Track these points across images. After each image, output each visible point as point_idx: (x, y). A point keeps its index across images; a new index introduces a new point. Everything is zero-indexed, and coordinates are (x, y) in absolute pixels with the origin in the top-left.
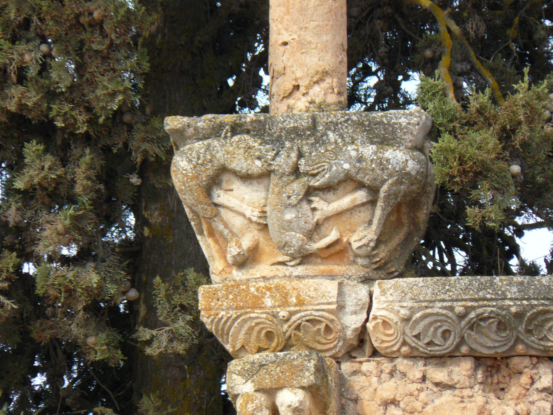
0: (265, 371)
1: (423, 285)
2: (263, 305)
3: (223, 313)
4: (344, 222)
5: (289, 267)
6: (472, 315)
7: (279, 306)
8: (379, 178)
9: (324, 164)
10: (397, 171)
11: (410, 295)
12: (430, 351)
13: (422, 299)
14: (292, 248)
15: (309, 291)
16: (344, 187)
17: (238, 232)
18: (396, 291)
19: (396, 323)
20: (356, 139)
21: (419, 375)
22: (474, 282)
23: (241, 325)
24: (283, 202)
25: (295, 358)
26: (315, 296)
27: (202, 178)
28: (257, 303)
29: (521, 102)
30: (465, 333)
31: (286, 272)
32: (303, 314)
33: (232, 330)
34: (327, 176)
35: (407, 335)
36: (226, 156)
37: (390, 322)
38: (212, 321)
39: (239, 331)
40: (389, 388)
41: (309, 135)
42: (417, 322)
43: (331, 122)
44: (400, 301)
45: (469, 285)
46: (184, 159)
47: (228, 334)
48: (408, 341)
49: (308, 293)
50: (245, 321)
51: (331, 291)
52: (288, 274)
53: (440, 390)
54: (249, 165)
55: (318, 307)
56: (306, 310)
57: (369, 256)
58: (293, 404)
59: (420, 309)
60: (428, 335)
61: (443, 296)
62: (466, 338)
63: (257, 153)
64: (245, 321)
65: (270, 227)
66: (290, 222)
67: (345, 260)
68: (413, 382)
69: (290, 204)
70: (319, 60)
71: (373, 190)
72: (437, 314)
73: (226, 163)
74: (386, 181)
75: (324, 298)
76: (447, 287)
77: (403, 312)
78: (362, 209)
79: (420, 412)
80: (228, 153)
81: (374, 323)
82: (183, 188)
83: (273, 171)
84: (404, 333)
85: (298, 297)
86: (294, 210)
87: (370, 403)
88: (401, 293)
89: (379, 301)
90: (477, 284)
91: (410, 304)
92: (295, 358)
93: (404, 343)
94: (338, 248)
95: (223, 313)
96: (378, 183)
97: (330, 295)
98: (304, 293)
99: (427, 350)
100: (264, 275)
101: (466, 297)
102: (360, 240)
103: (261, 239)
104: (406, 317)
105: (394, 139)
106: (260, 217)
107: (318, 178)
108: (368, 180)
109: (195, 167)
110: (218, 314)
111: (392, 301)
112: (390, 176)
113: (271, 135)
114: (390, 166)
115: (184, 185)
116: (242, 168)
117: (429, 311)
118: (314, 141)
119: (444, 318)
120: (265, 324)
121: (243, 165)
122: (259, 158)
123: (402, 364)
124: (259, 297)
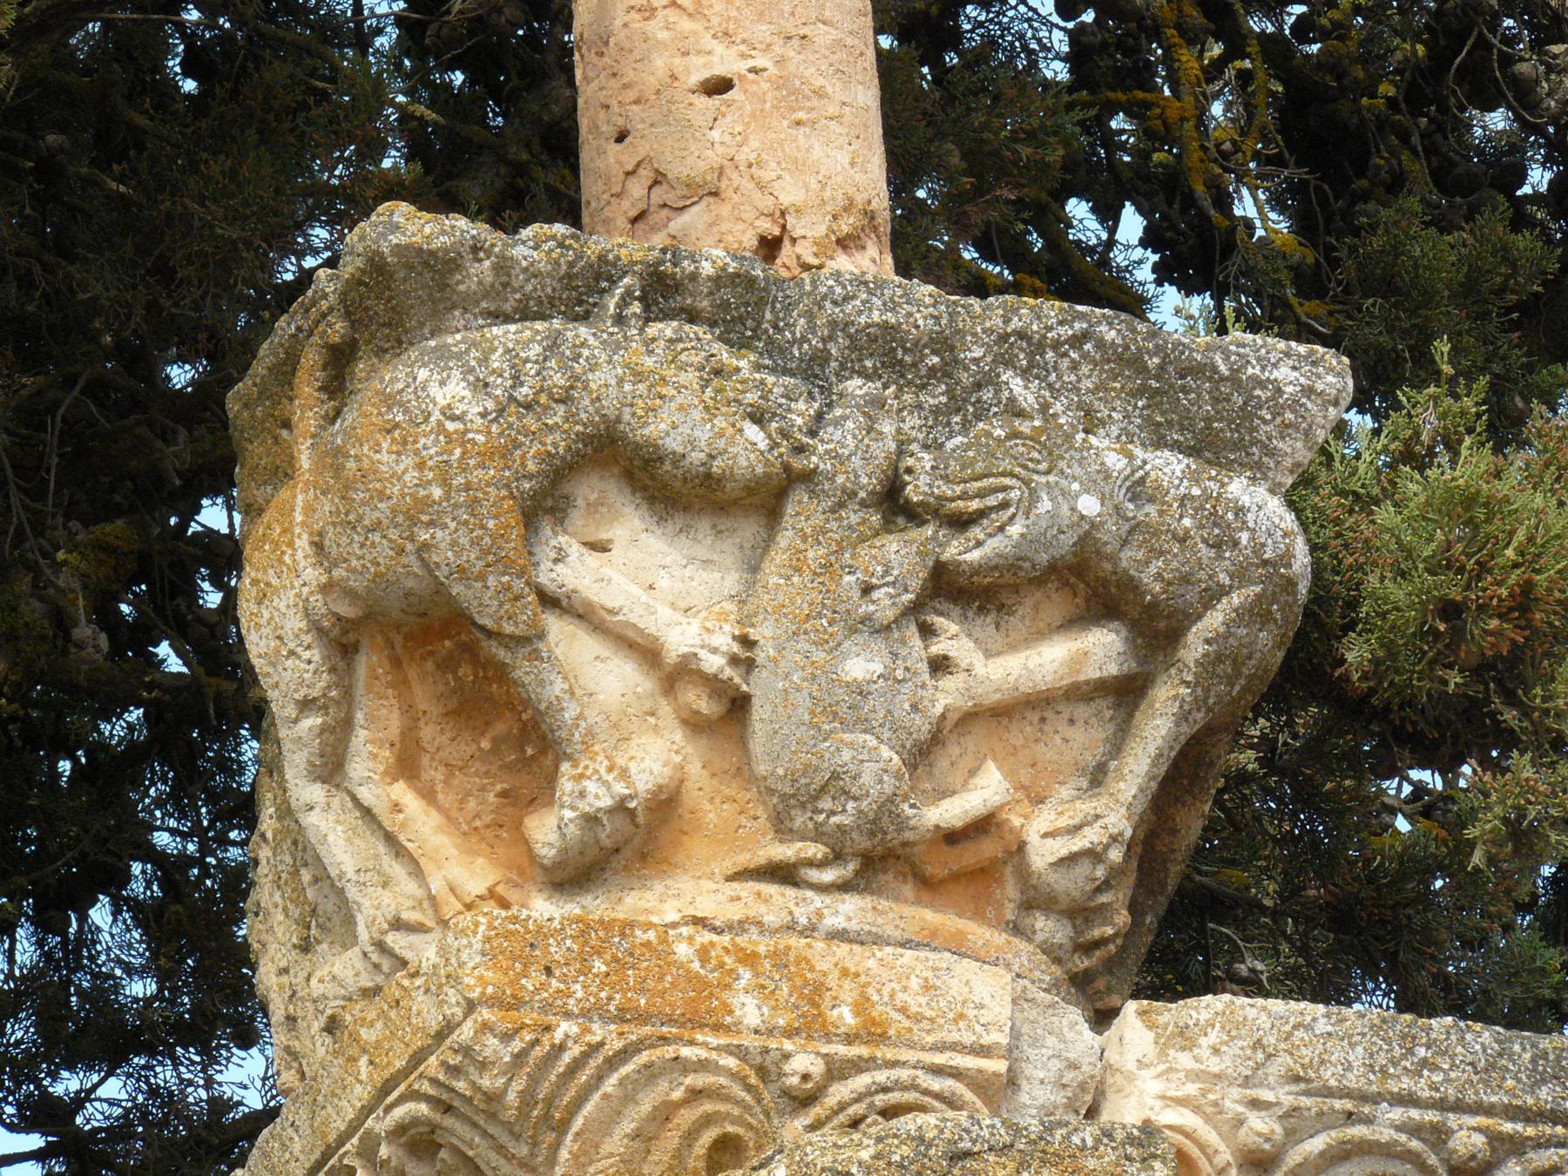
1: (1329, 1028)
2: (729, 1019)
3: (565, 1028)
4: (1015, 751)
5: (809, 894)
7: (790, 1033)
8: (1202, 575)
9: (1008, 481)
10: (1265, 563)
13: (1333, 1083)
14: (851, 805)
15: (905, 989)
16: (1036, 608)
17: (605, 725)
18: (1232, 1038)
20: (1103, 423)
22: (1517, 1048)
23: (628, 1094)
24: (841, 608)
25: (1090, 1142)
26: (929, 1013)
27: (523, 457)
28: (703, 1015)
31: (797, 912)
32: (881, 1076)
33: (589, 1107)
34: (1015, 530)
36: (627, 387)
37: (1203, 1163)
38: (519, 1057)
39: (613, 1115)
41: (932, 370)
43: (1021, 335)
44: (1247, 1082)
45: (1501, 1055)
46: (457, 374)
49: (901, 997)
50: (650, 1073)
51: (987, 1001)
52: (803, 921)
54: (721, 435)
55: (940, 1059)
56: (894, 1064)
57: (1080, 913)
59: (1324, 1121)
61: (1406, 1083)
63: (751, 397)
64: (650, 1073)
65: (760, 713)
66: (860, 691)
67: (990, 913)
69: (866, 619)
70: (852, 164)
71: (1156, 631)
73: (627, 417)
74: (1224, 591)
75: (962, 1024)
76: (1421, 1052)
77: (1259, 1123)
78: (1082, 711)
80: (639, 376)
82: (437, 492)
83: (808, 477)
85: (862, 1006)
86: (879, 644)
88: (1254, 1048)
89: (1170, 1070)
90: (1527, 1056)
91: (1286, 1096)
92: (1090, 1142)
94: (987, 848)
95: (565, 1028)
96: (1192, 595)
97: (986, 1016)
98: (886, 991)
100: (700, 915)
101: (1494, 1099)
103: (695, 769)
104: (1267, 1146)
105: (1237, 446)
106: (734, 660)
107: (976, 532)
108: (1159, 577)
109: (501, 411)
110: (548, 1028)
112: (1240, 576)
113: (782, 351)
114: (1244, 537)
115: (445, 483)
116: (692, 443)
117: (1358, 1131)
118: (944, 399)
120: (727, 1098)
121: (697, 433)
122: (758, 418)
124: (707, 984)
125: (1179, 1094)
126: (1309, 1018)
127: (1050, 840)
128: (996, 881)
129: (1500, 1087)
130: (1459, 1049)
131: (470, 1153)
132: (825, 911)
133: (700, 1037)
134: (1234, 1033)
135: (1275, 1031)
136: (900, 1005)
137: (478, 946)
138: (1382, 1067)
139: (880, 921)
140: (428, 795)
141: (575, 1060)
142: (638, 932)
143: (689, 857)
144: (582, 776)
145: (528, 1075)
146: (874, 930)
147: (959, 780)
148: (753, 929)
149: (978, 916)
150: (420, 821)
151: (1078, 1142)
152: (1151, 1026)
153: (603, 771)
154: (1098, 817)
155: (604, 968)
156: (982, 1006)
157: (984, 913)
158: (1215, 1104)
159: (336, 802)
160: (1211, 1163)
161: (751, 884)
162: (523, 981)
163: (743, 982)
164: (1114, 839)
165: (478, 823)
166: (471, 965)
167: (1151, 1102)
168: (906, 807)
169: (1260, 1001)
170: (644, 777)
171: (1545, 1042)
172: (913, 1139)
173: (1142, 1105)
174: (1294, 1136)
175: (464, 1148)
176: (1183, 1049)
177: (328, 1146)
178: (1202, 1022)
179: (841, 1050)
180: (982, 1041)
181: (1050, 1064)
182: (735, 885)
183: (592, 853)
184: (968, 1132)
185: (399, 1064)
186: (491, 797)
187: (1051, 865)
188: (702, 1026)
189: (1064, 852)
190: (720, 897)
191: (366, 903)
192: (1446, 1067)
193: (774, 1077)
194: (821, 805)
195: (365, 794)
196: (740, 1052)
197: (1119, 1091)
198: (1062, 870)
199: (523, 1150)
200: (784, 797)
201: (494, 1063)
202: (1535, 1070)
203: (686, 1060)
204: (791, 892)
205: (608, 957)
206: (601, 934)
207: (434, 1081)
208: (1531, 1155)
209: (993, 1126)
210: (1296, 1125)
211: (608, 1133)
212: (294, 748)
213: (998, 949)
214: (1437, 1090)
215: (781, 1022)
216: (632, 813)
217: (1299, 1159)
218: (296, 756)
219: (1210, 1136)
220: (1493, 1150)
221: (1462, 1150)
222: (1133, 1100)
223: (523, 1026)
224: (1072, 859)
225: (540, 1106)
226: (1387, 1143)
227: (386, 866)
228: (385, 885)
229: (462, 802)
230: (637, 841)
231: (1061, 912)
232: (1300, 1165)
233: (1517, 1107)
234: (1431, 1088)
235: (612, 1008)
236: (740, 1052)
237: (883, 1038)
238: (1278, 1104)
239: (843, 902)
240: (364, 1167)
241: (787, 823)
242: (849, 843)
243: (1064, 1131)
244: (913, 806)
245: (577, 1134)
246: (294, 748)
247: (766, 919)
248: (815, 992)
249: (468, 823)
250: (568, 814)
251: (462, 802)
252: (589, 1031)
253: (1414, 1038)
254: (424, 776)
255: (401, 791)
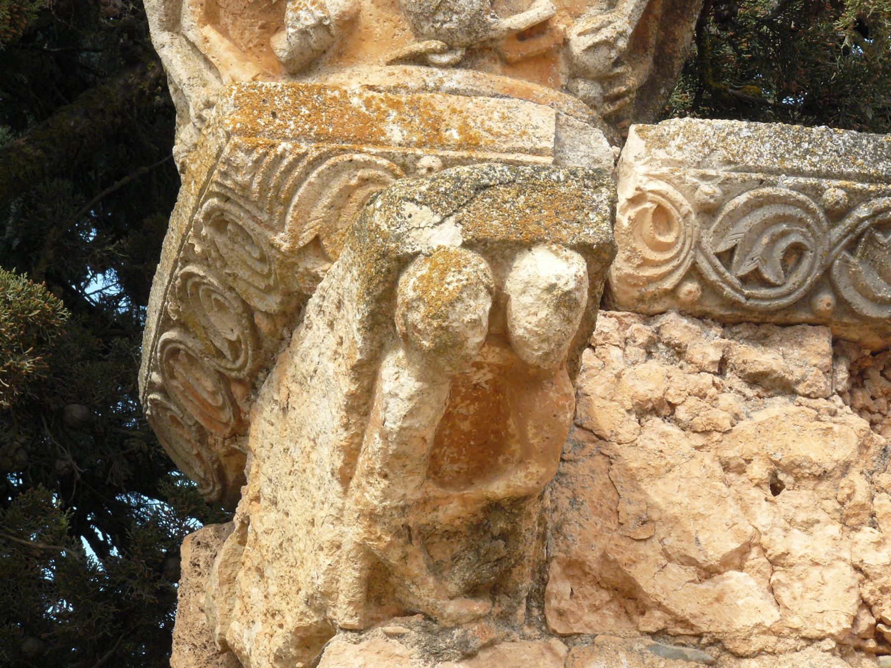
0: (489, 200)
1: (749, 134)
2: (383, 138)
3: (283, 146)
5: (435, 70)
6: (863, 211)
7: (420, 145)
11: (721, 153)
12: (748, 298)
13: (751, 164)
14: (455, 17)
15: (490, 119)
19: (686, 217)
21: (715, 355)
22: (865, 142)
25: (562, 178)
26: (504, 132)
29: (346, 284)
30: (836, 258)
31: (428, 80)
33: (301, 191)
35: (703, 251)
37: (674, 212)
38: (257, 162)
40: (651, 378)
42: (736, 216)
45: (854, 146)
47: (287, 202)
48: (704, 265)
50: (337, 170)
51: (540, 124)
52: (432, 85)
53: (758, 395)
57: (605, 79)
58: (561, 284)
59: (746, 185)
60: (751, 256)
61: (796, 163)
62: (835, 271)
68: (702, 370)
72: (784, 201)
75: (524, 137)
76: (806, 145)
79: (725, 433)
81: (632, 212)
84: (698, 245)
85: (464, 129)
87: (606, 403)
88: (703, 146)
89: (652, 160)
90: (871, 146)
91: (722, 172)
92: (562, 178)
93: (694, 273)
94: (544, 43)
95: (283, 146)
97: (539, 133)
98: (479, 121)
99: (741, 293)
100: (370, 84)
101: (850, 170)
102: (597, 30)
104: (712, 201)
110: (273, 146)
111: (681, 163)
119: (797, 212)
123: (676, 327)
124: (370, 120)
125: (657, 173)
126: (737, 129)
127: (582, 37)
128: (554, 62)
129: (854, 163)
130: (829, 143)
131: (240, 223)
132: (445, 79)
133: (365, 149)
134: (691, 138)
135: (716, 136)
136: (486, 127)
137: (231, 102)
138: (781, 154)
139: (478, 83)
140: (224, 33)
141: (290, 163)
142: (328, 92)
143: (366, 54)
144: (297, 9)
145: (263, 172)
146: (474, 88)
147: (525, 5)
148: (403, 91)
149: (543, 82)
150: (218, 45)
151: (555, 178)
152: (644, 138)
153: (309, 5)
154: (610, 22)
155: (307, 112)
156: (537, 128)
157: (546, 80)
158: (680, 178)
159: (177, 42)
160: (679, 211)
161: (401, 66)
162: (259, 121)
163: (392, 118)
164: (621, 34)
165: (251, 45)
166: (228, 113)
167: (640, 178)
168: (488, 17)
169: (707, 121)
170: (334, 7)
171: (882, 139)
172: (454, 179)
173: (636, 180)
174: (728, 195)
175: (237, 221)
176: (660, 148)
177: (183, 235)
178: (671, 132)
179: (451, 153)
180: (537, 147)
181: (583, 160)
182: (392, 67)
183: (308, 53)
184: (487, 174)
185: (204, 178)
186: (256, 29)
187: (584, 51)
188: (367, 143)
189: (590, 43)
190: (383, 74)
191: (193, 95)
192: (821, 153)
193: (412, 170)
194: (438, 17)
195: (191, 35)
196: (389, 156)
197: (626, 175)
198: (590, 54)
199: (265, 217)
200: (416, 15)
201: (243, 167)
202: (875, 154)
203: (357, 162)
204: (424, 69)
205: (310, 106)
206: (306, 93)
207: (217, 183)
208: (874, 201)
209: (503, 171)
210: (729, 188)
211: (314, 205)
212: (151, 13)
213: (553, 99)
214: (815, 166)
215: (415, 139)
216: (327, 28)
217: (732, 207)
218: (153, 18)
219: (678, 197)
220: (850, 199)
221: (831, 199)
222: (632, 179)
223: (258, 145)
224: (595, 47)
225: (272, 191)
226: (784, 196)
227: (205, 75)
228: (204, 85)
229: (242, 34)
230: (335, 47)
231: (594, 79)
232: (733, 211)
233: (866, 175)
234: (811, 165)
235: (312, 134)
236: (389, 156)
237: (477, 146)
238: (718, 177)
239: (456, 73)
240: (198, 243)
241: (420, 30)
242: (456, 39)
243: (547, 172)
244: (493, 17)
245: (295, 206)
246: (151, 13)
247: (410, 85)
248: (435, 125)
249: (246, 46)
250: (291, 30)
251: (242, 34)
252: (299, 147)
253: (801, 138)
254: (222, 22)
255: (209, 31)
